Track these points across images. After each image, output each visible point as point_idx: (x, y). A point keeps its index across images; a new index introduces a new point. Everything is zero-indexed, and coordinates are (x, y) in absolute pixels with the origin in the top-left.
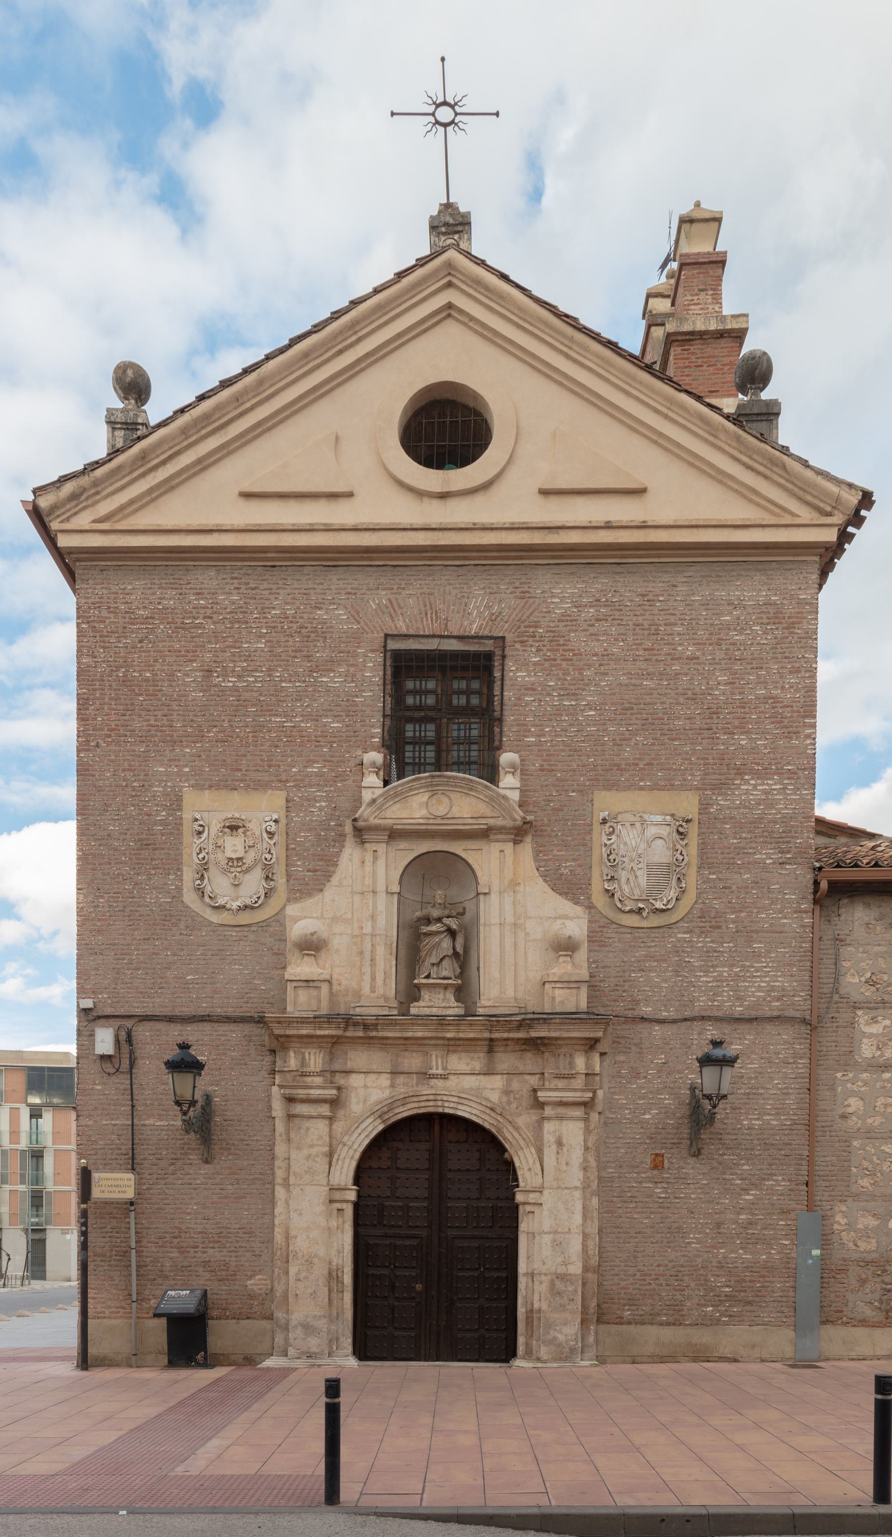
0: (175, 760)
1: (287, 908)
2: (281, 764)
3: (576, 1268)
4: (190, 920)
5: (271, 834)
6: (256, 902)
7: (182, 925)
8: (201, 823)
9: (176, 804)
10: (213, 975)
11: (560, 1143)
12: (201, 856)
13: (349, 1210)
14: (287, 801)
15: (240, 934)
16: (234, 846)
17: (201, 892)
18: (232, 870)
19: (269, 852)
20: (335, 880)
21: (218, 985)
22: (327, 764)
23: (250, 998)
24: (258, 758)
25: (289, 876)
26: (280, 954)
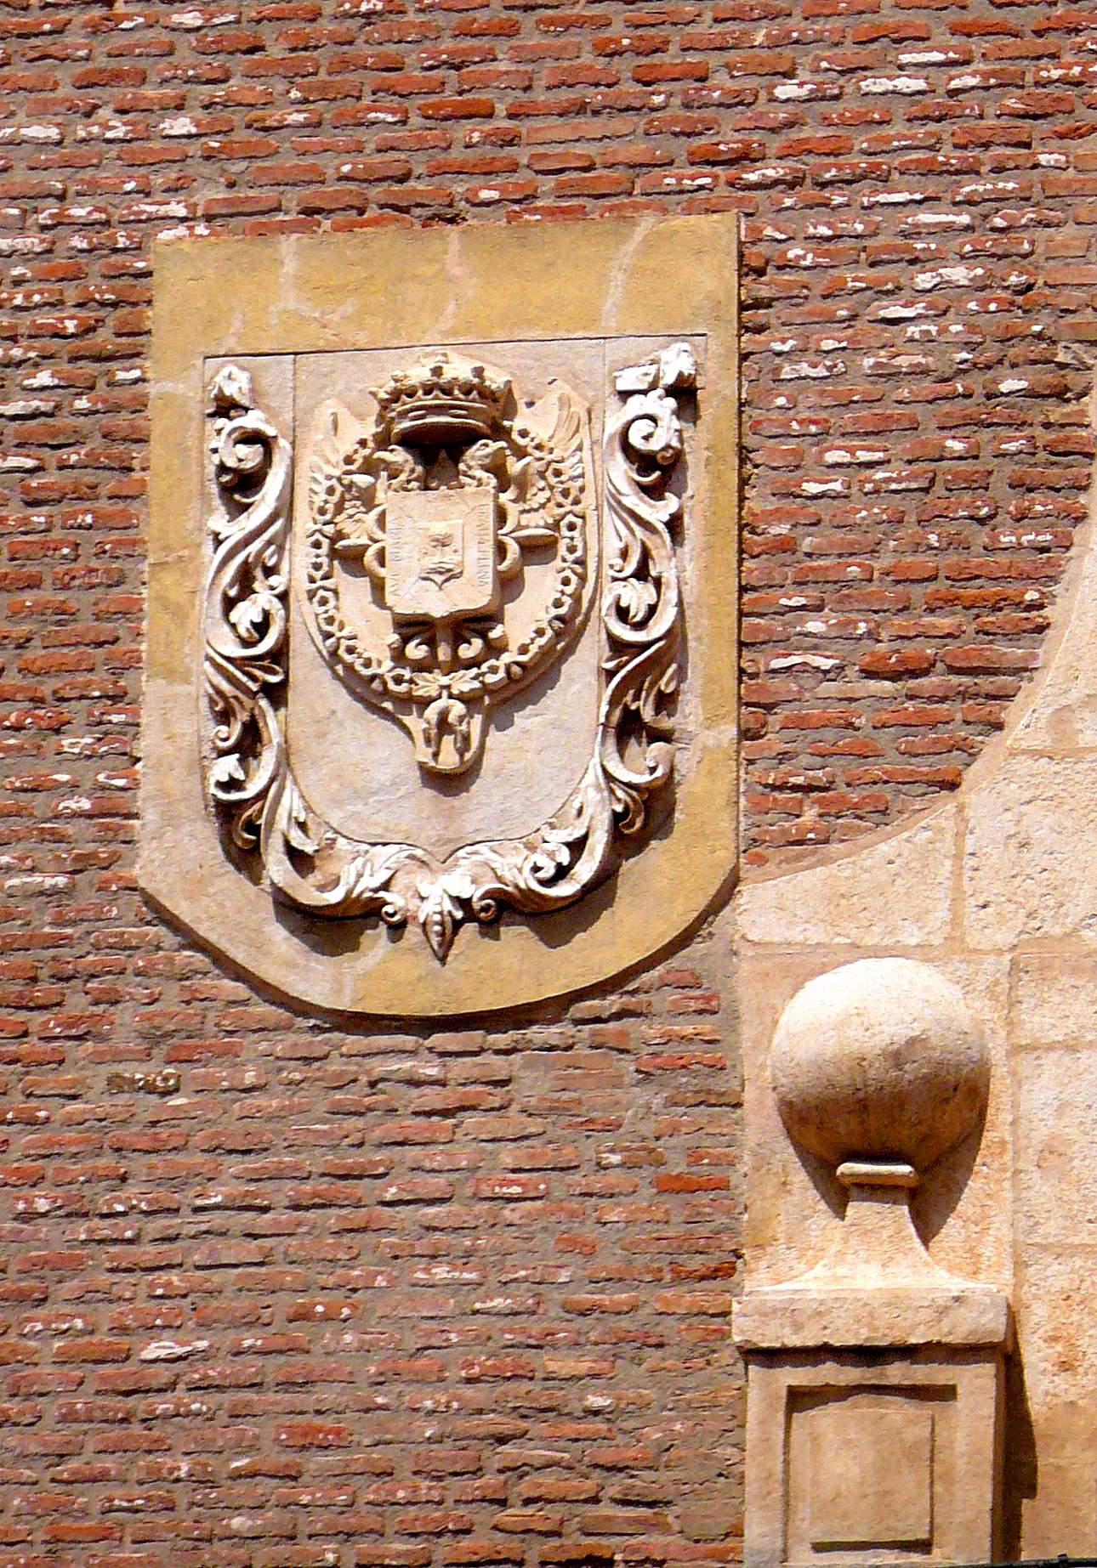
0: (117, 77)
1: (746, 895)
2: (714, 60)
4: (172, 994)
5: (659, 471)
6: (562, 872)
7: (126, 1021)
8: (252, 421)
9: (109, 322)
10: (300, 1332)
12: (247, 614)
14: (749, 269)
15: (461, 1068)
16: (437, 543)
17: (239, 830)
18: (428, 684)
19: (641, 574)
21: (327, 1395)
22: (978, 45)
23: (517, 1470)
24: (583, 38)
25: (755, 714)
26: (702, 1183)
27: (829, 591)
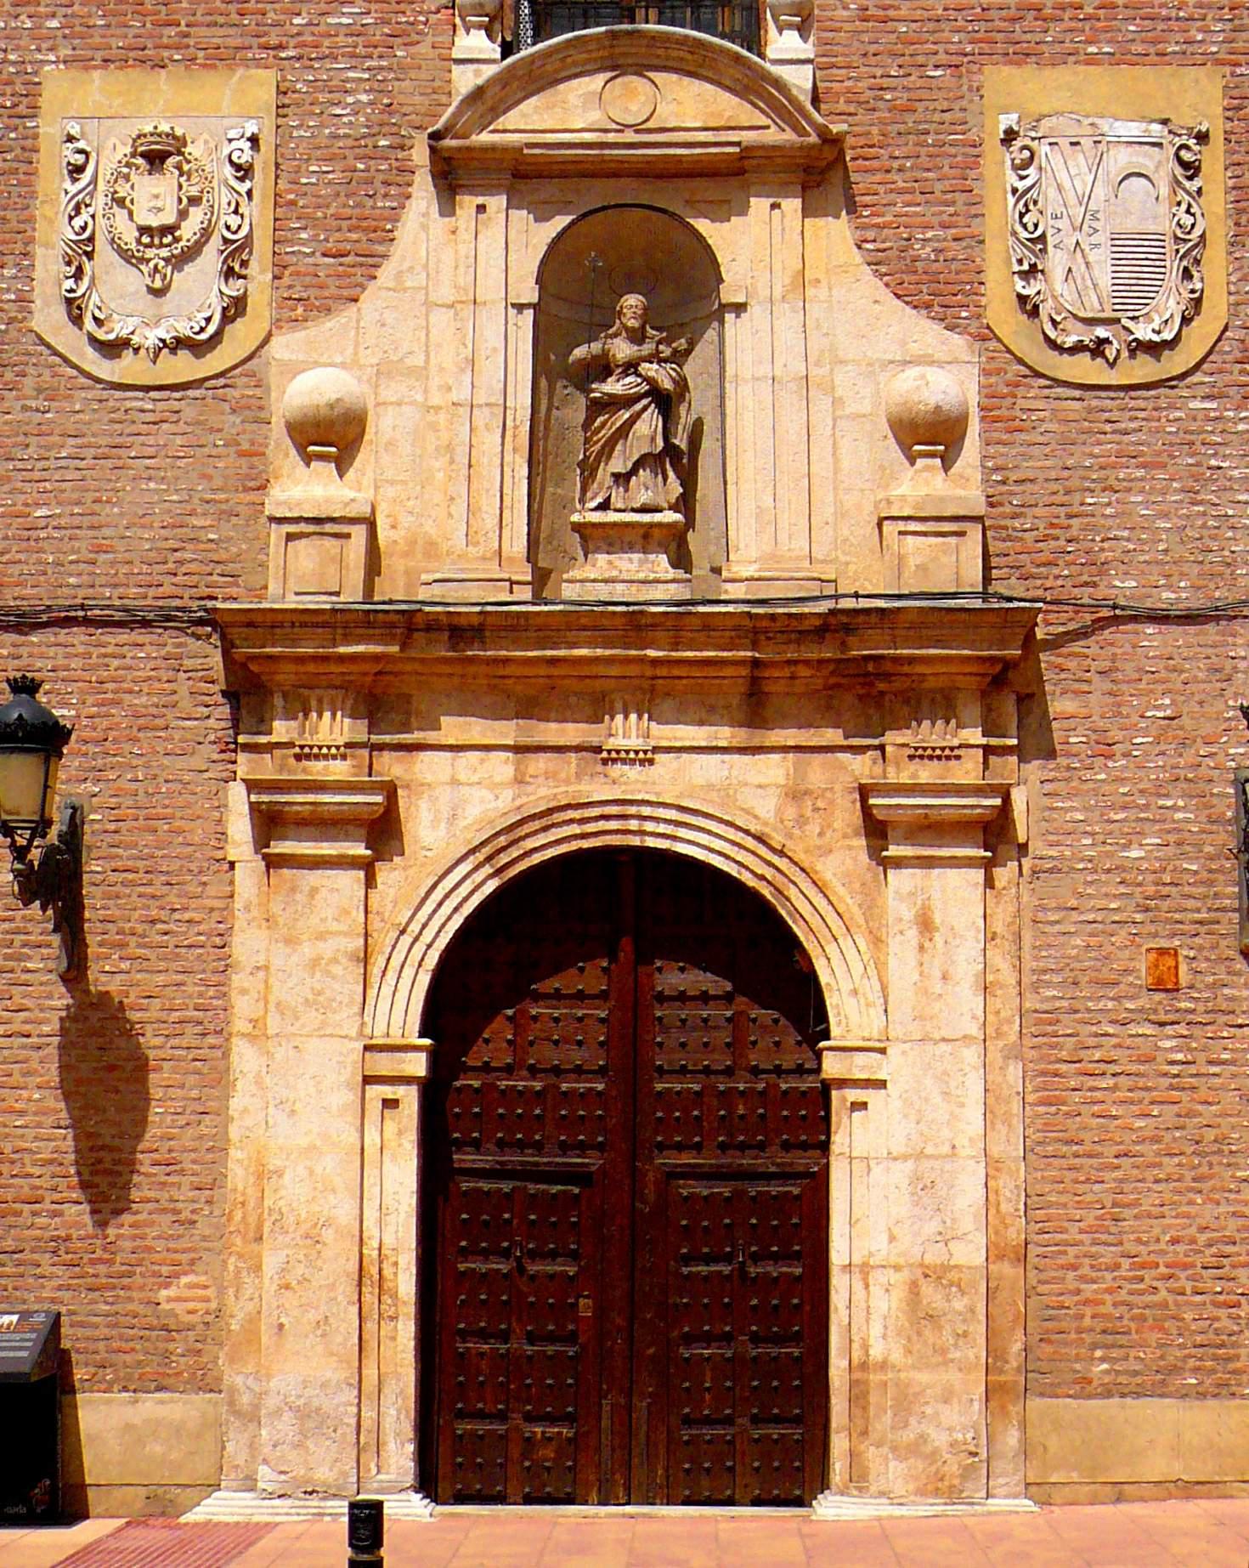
3: (970, 1253)
7: (29, 383)
11: (925, 924)
13: (410, 1097)
20: (386, 274)
27: (309, 222)
